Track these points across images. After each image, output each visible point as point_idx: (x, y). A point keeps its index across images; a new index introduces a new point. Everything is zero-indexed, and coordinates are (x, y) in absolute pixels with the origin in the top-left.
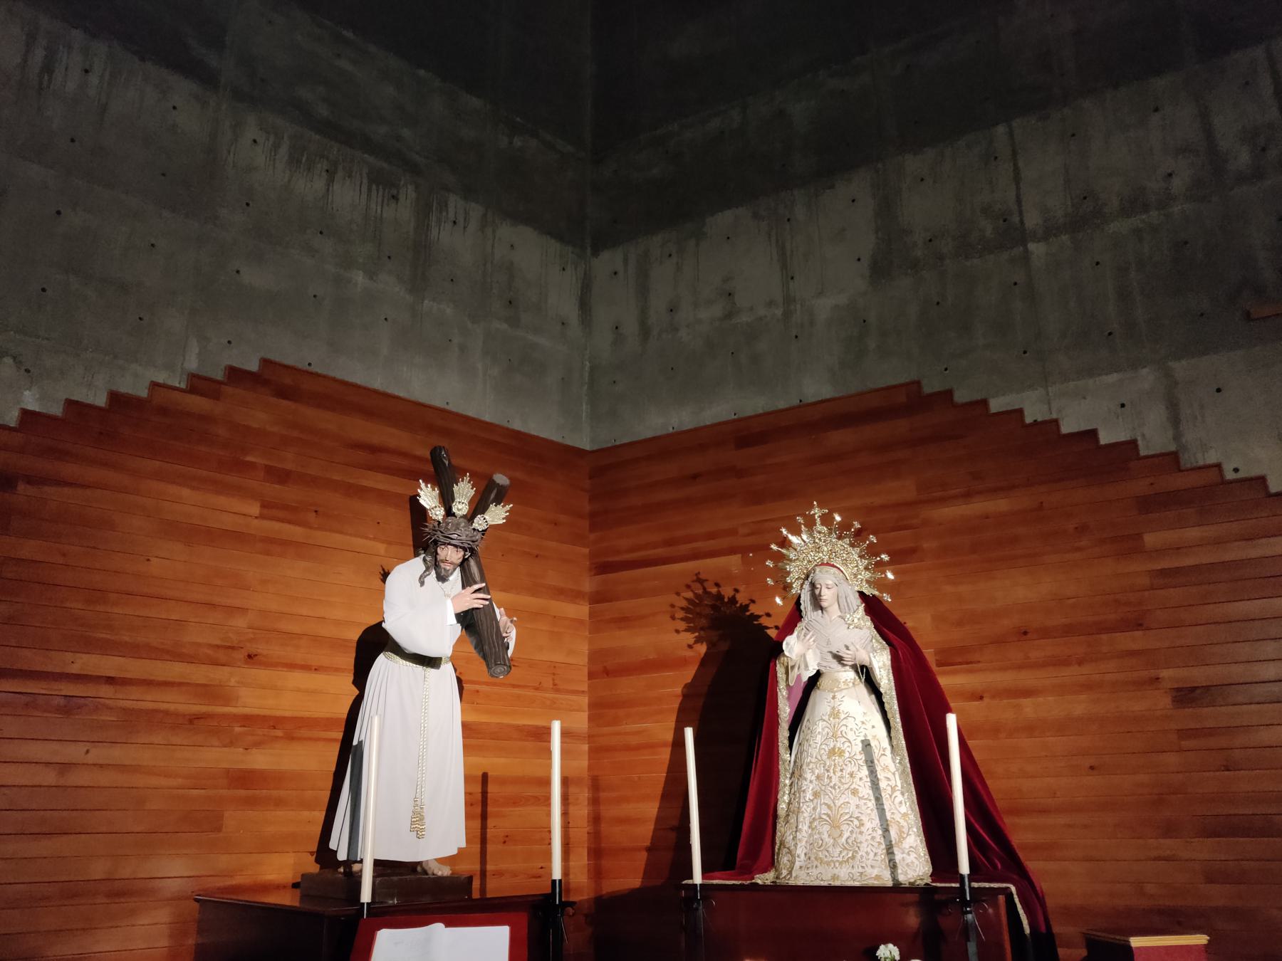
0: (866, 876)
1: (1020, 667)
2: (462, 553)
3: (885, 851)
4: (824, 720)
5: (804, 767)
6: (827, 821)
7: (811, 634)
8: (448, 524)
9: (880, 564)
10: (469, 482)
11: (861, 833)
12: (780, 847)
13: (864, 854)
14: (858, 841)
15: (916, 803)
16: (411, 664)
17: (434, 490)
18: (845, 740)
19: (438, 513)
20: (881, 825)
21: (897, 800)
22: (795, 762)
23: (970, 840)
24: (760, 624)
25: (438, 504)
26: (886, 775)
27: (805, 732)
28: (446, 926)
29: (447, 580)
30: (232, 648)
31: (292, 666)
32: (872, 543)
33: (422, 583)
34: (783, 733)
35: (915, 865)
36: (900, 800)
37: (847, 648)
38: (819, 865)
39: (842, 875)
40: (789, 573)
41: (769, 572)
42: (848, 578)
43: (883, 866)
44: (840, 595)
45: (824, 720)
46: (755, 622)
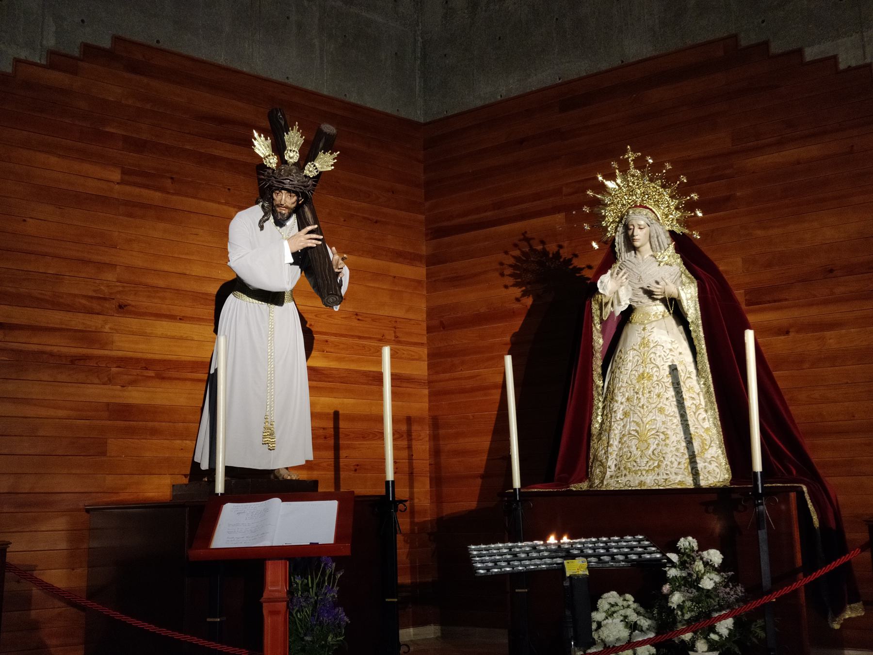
0: (670, 481)
1: (826, 302)
2: (295, 198)
3: (688, 460)
4: (635, 350)
5: (616, 391)
6: (635, 436)
7: (623, 271)
8: (281, 171)
9: (691, 206)
10: (298, 131)
11: (666, 445)
12: (593, 461)
13: (669, 463)
14: (664, 452)
15: (718, 419)
16: (257, 301)
17: (266, 139)
18: (654, 365)
19: (271, 161)
20: (685, 438)
21: (701, 417)
22: (608, 387)
23: (762, 439)
24: (582, 276)
25: (271, 153)
26: (691, 395)
27: (618, 361)
28: (283, 501)
29: (284, 225)
30: (105, 299)
31: (159, 316)
32: (682, 182)
33: (262, 228)
34: (598, 363)
35: (716, 473)
36: (704, 417)
37: (657, 283)
38: (627, 473)
39: (649, 482)
40: (605, 217)
41: (587, 218)
42: (660, 218)
43: (686, 474)
44: (652, 235)
45: (635, 350)
46: (577, 275)
